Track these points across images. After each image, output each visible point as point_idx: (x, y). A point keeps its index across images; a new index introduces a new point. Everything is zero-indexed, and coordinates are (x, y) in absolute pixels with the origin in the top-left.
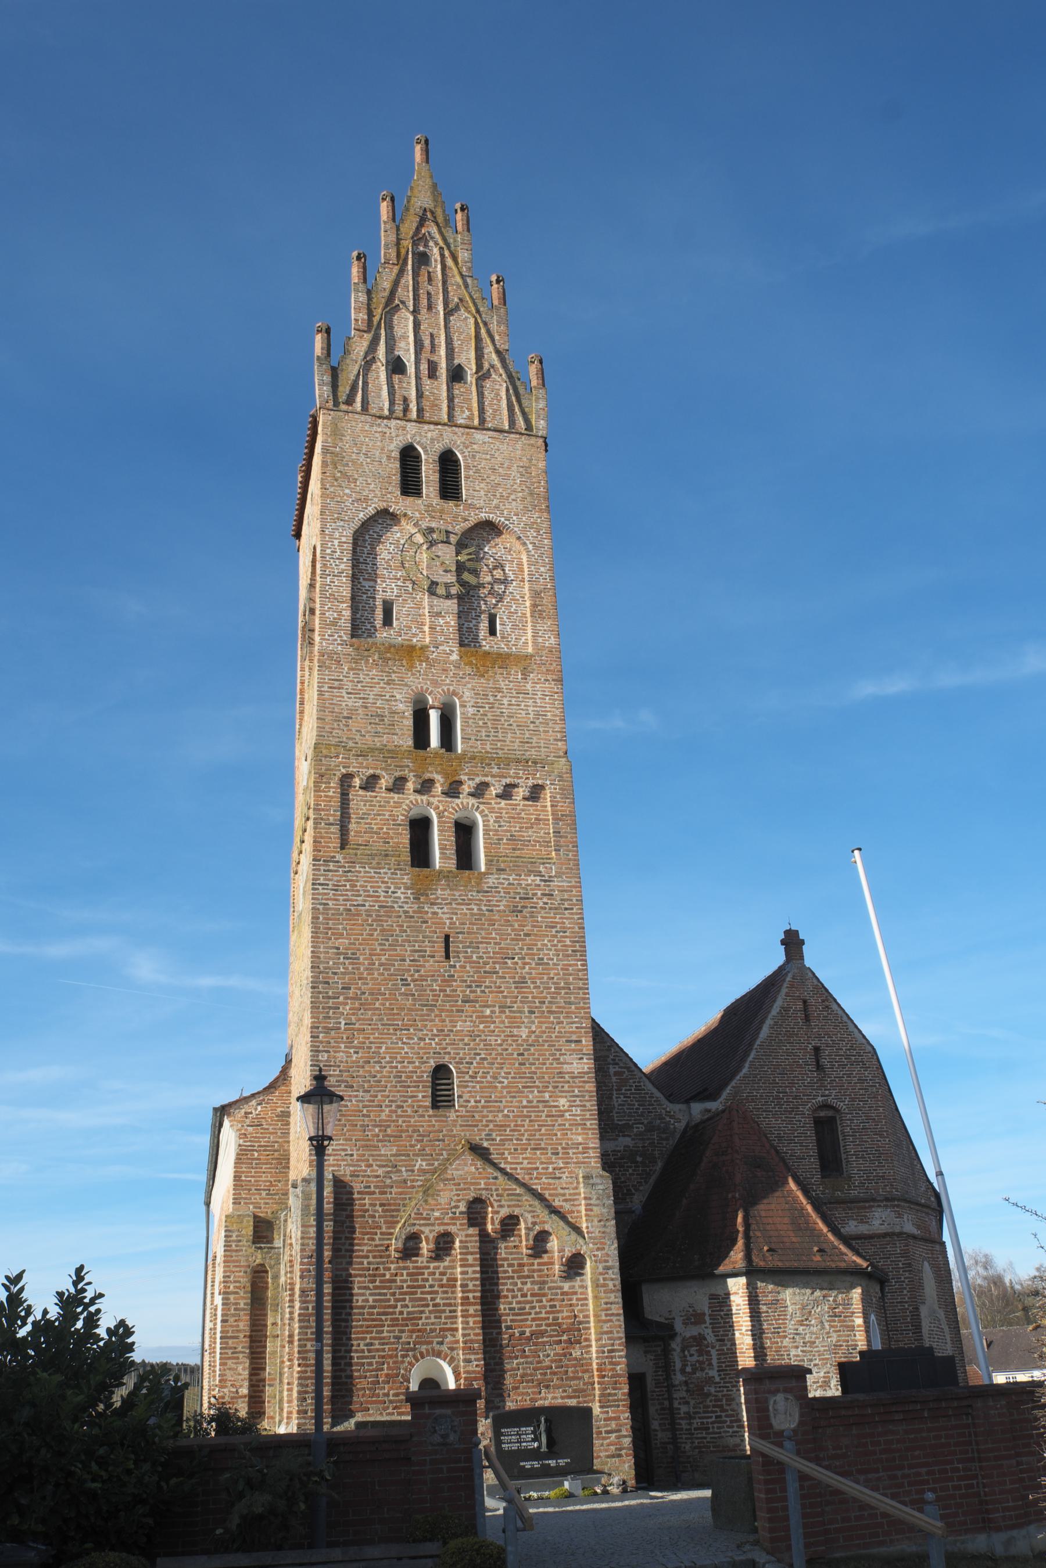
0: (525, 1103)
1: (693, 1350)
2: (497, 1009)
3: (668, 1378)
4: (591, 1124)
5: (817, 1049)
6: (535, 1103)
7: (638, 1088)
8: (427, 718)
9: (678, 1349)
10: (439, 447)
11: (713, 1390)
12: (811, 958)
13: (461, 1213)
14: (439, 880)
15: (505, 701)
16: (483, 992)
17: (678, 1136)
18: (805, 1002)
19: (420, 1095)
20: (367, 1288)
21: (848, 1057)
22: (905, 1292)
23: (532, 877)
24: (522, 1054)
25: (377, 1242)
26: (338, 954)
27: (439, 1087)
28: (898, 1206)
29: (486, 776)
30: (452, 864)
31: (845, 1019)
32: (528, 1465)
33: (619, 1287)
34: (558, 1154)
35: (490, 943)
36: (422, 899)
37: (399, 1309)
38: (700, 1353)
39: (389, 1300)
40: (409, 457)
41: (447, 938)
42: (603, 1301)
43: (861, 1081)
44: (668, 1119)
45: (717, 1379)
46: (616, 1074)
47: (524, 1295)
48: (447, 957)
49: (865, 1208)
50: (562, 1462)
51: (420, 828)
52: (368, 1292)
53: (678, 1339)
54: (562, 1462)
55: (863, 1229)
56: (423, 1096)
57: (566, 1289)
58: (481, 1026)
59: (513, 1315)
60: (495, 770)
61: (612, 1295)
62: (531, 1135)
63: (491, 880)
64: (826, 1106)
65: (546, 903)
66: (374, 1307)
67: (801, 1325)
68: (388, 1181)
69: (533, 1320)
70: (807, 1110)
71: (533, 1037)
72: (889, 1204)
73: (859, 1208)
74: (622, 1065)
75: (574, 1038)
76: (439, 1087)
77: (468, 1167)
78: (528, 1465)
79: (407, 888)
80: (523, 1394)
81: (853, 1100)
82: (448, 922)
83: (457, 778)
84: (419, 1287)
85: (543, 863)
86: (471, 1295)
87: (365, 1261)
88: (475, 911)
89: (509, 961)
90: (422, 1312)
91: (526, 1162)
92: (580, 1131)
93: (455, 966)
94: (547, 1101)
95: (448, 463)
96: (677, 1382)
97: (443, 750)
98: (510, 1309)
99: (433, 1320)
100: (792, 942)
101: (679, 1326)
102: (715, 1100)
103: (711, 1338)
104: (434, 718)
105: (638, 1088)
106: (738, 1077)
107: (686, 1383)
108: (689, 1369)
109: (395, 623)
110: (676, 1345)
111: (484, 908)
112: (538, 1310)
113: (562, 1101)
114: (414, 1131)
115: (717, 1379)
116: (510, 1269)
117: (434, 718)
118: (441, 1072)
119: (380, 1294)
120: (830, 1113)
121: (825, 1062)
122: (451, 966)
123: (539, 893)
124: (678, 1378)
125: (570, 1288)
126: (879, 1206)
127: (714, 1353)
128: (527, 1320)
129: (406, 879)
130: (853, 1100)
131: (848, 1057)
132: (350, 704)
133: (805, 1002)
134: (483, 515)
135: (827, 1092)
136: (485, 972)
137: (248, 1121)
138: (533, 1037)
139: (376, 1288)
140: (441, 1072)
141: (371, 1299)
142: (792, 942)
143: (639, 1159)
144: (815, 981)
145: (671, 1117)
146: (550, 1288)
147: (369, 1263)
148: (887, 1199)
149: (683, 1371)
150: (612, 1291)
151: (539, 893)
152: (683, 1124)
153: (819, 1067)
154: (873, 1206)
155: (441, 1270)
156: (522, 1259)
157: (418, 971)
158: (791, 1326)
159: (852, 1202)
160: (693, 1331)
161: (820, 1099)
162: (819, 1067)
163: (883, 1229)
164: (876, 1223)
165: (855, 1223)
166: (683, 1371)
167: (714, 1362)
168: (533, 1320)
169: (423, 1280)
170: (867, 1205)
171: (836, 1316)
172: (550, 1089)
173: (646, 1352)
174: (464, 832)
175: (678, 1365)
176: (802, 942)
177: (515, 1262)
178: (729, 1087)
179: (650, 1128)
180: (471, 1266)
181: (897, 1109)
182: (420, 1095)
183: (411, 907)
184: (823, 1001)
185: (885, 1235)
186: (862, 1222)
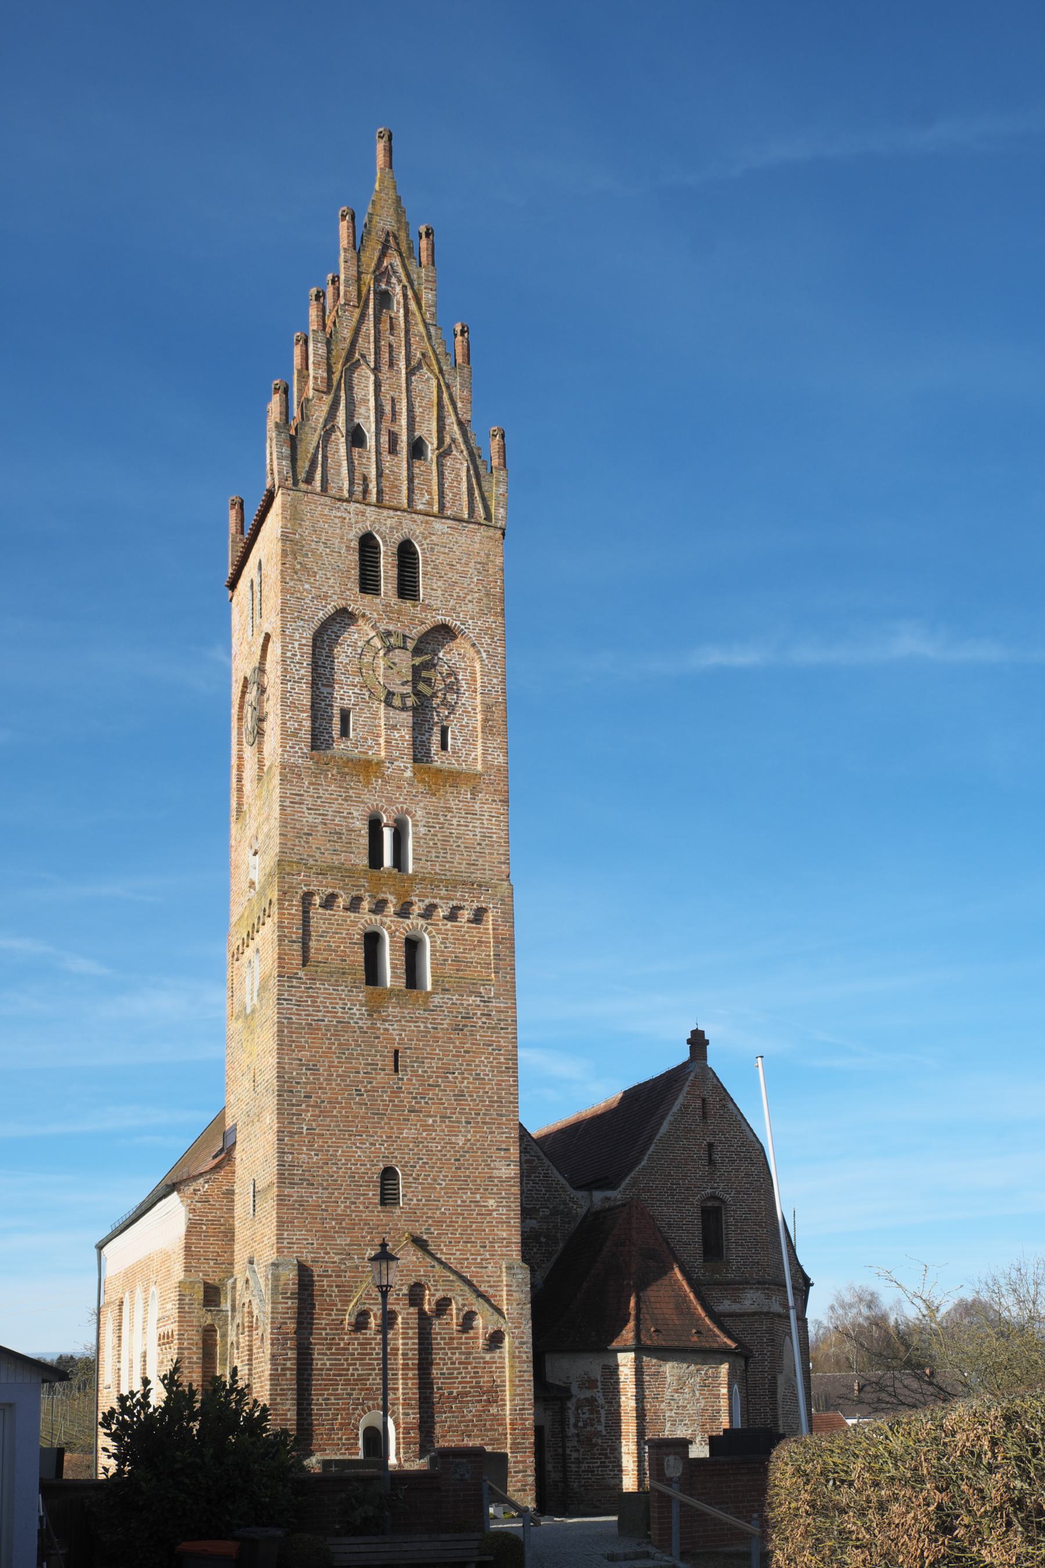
0: (459, 1203)
1: (585, 1409)
2: (438, 1119)
5: (710, 1146)
6: (468, 1203)
9: (573, 1408)
10: (398, 537)
11: (599, 1441)
13: (404, 1295)
14: (391, 998)
17: (579, 1220)
18: (704, 1100)
19: (371, 1193)
22: (766, 1363)
23: (473, 998)
24: (458, 1160)
25: (334, 1317)
28: (768, 1289)
29: (435, 898)
30: (402, 983)
33: (531, 1359)
34: (485, 1247)
35: (434, 1059)
38: (591, 1412)
39: (343, 1364)
40: (367, 545)
41: (396, 1052)
42: (517, 1369)
43: (747, 1175)
44: (571, 1205)
45: (604, 1433)
47: (453, 1363)
48: (396, 1070)
49: (739, 1289)
51: (372, 941)
52: (326, 1357)
53: (574, 1400)
55: (736, 1308)
56: (373, 1194)
57: (487, 1359)
58: (424, 1134)
60: (443, 892)
61: (525, 1365)
62: (463, 1230)
63: (437, 1000)
64: (713, 1197)
65: (485, 1023)
67: (677, 1393)
69: (460, 1383)
70: (696, 1200)
71: (468, 1145)
72: (760, 1286)
73: (733, 1289)
74: (532, 1153)
81: (738, 1192)
82: (397, 1038)
83: (408, 899)
84: (368, 1354)
85: (484, 985)
86: (410, 1362)
87: (324, 1333)
88: (422, 1028)
89: (450, 1076)
90: (370, 1374)
92: (505, 1228)
93: (402, 1079)
94: (478, 1202)
95: (406, 553)
98: (441, 1374)
101: (574, 1390)
102: (614, 1188)
103: (601, 1400)
104: (387, 834)
106: (637, 1169)
107: (578, 1435)
108: (581, 1424)
110: (571, 1405)
112: (463, 1375)
113: (491, 1202)
114: (365, 1224)
115: (604, 1433)
116: (442, 1342)
117: (387, 834)
118: (389, 1174)
119: (335, 1359)
120: (717, 1204)
121: (717, 1157)
122: (399, 1079)
124: (572, 1431)
126: (752, 1288)
127: (603, 1412)
128: (455, 1383)
129: (361, 997)
130: (738, 1192)
133: (704, 1100)
134: (439, 617)
135: (716, 1185)
137: (197, 1198)
138: (468, 1145)
139: (332, 1354)
140: (389, 1174)
141: (328, 1363)
143: (543, 1240)
144: (715, 1080)
146: (474, 1358)
148: (759, 1283)
149: (576, 1426)
150: (525, 1362)
151: (479, 1013)
152: (585, 1210)
153: (711, 1162)
154: (746, 1288)
156: (453, 1334)
157: (371, 1083)
158: (668, 1393)
159: (728, 1284)
160: (588, 1394)
161: (709, 1191)
162: (711, 1162)
163: (754, 1308)
164: (748, 1303)
165: (729, 1302)
166: (576, 1426)
167: (603, 1419)
168: (460, 1383)
169: (371, 1349)
170: (741, 1287)
171: (705, 1386)
172: (481, 1191)
174: (412, 947)
175: (572, 1421)
177: (447, 1336)
178: (628, 1178)
180: (411, 1338)
182: (371, 1193)
184: (721, 1100)
185: (754, 1314)
186: (735, 1301)
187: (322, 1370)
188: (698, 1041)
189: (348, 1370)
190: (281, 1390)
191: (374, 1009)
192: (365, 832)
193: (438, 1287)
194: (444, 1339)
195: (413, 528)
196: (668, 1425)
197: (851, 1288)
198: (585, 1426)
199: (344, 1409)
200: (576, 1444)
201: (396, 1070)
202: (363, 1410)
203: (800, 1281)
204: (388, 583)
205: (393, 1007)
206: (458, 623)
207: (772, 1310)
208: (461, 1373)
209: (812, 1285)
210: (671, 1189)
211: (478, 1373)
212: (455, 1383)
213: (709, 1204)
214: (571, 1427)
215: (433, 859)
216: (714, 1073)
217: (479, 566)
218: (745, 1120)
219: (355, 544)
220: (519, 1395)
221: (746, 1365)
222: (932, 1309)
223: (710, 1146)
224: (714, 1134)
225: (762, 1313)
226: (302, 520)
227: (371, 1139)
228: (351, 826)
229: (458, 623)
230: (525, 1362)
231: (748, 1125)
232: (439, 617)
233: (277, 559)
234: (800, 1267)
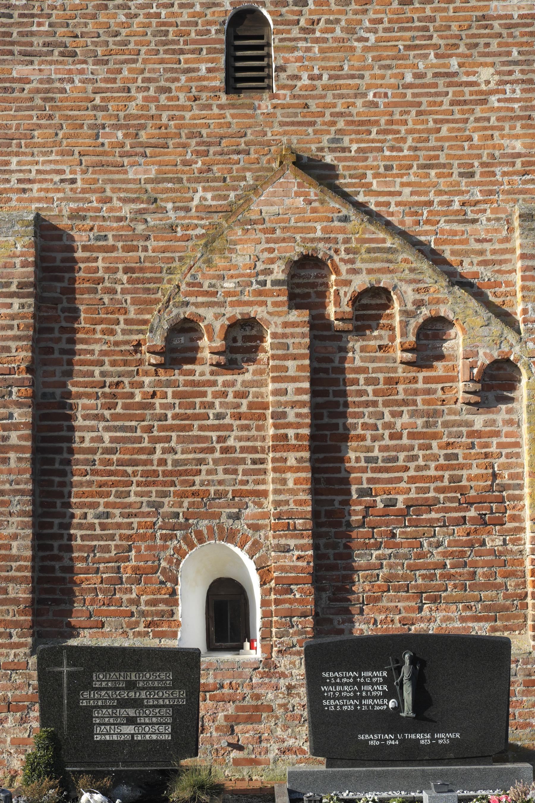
0: (409, 78)
6: (429, 79)
37: (158, 455)
39: (140, 440)
50: (443, 738)
54: (443, 738)
59: (374, 470)
66: (113, 451)
69: (412, 480)
84: (197, 417)
87: (97, 371)
91: (407, 191)
114: (191, 135)
119: (123, 429)
128: (400, 480)
168: (412, 480)
182: (203, 67)
189: (153, 451)
194: (374, 381)
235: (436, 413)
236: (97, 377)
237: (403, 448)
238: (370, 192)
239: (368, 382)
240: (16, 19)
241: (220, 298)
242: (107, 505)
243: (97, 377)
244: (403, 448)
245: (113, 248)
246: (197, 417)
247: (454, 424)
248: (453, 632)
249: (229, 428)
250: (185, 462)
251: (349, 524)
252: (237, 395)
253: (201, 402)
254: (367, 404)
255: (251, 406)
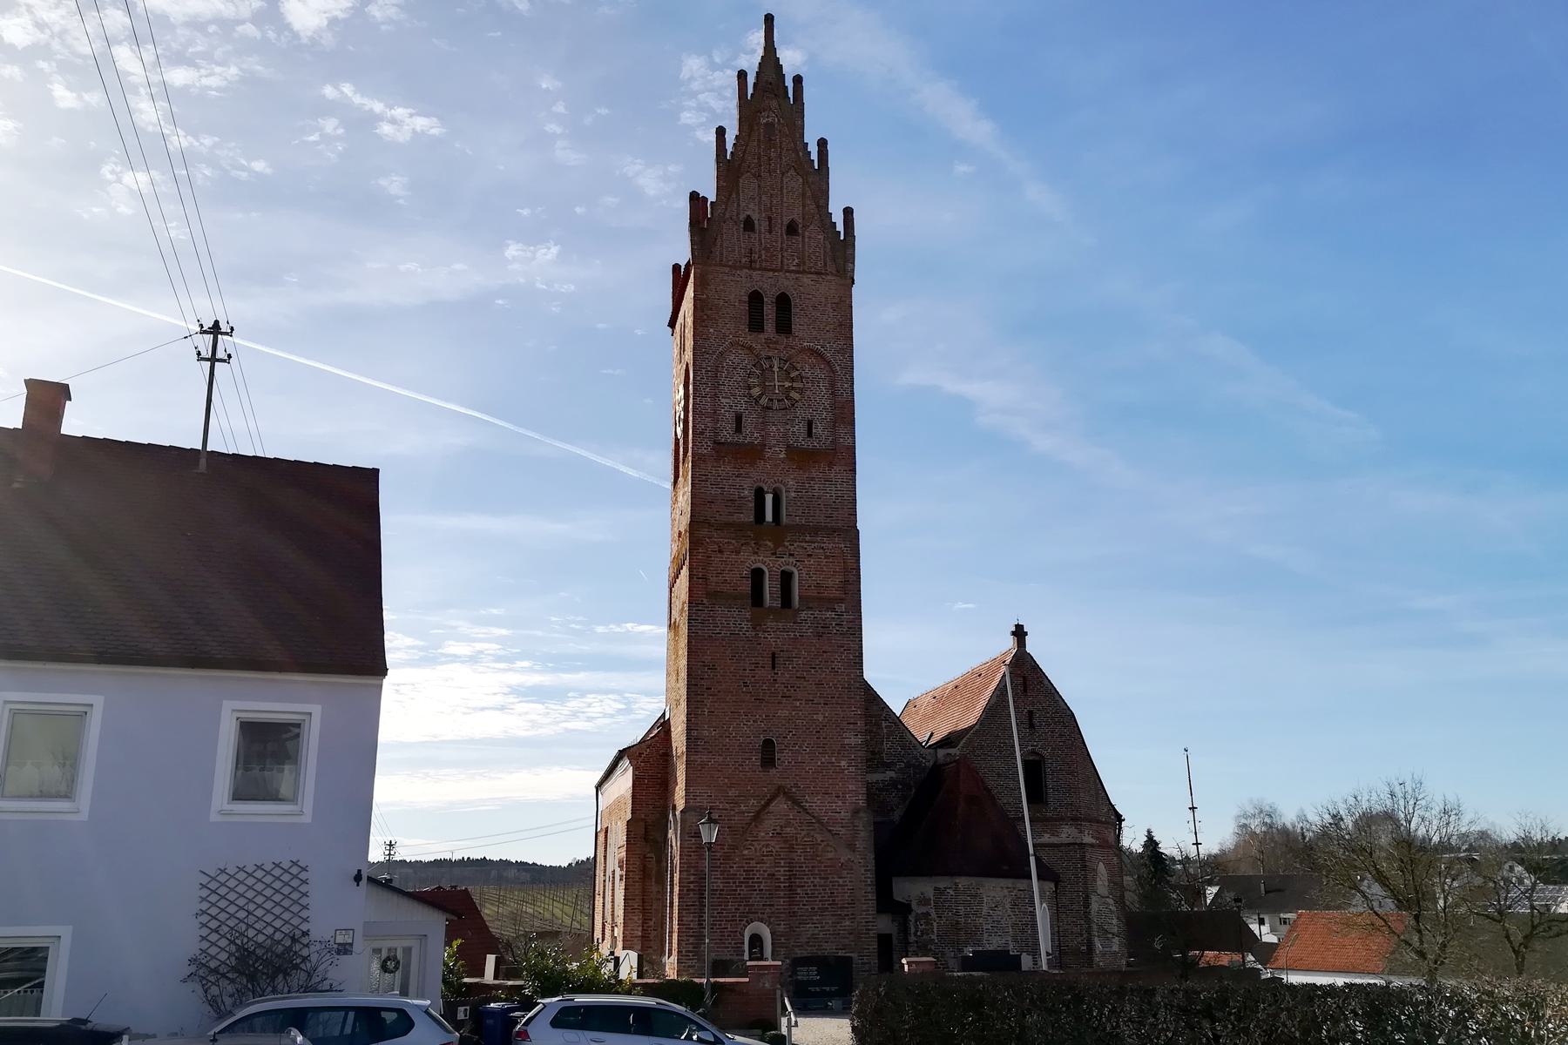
0: (819, 764)
1: (922, 922)
2: (803, 702)
3: (906, 938)
4: (784, 902)
5: (1031, 713)
6: (826, 764)
7: (901, 737)
8: (764, 500)
9: (913, 920)
10: (775, 292)
11: (933, 947)
12: (1030, 648)
15: (816, 487)
16: (795, 690)
17: (927, 771)
19: (754, 758)
20: (719, 878)
21: (1052, 718)
25: (726, 850)
26: (704, 666)
27: (769, 517)
29: (802, 542)
30: (778, 604)
31: (1053, 691)
32: (812, 989)
33: (874, 883)
36: (758, 628)
37: (738, 892)
38: (927, 923)
39: (732, 886)
40: (755, 298)
41: (774, 654)
44: (921, 759)
45: (936, 941)
46: (886, 727)
47: (815, 886)
48: (774, 668)
50: (833, 989)
51: (757, 575)
53: (913, 914)
54: (833, 989)
55: (1055, 840)
56: (756, 759)
57: (841, 883)
58: (794, 713)
59: (808, 897)
60: (808, 538)
61: (870, 888)
63: (803, 615)
66: (723, 890)
68: (732, 813)
69: (820, 901)
74: (890, 721)
75: (852, 726)
76: (769, 517)
77: (780, 805)
78: (812, 989)
79: (747, 621)
80: (811, 946)
84: (751, 879)
87: (719, 862)
89: (813, 670)
90: (753, 894)
91: (819, 801)
93: (777, 674)
95: (783, 302)
96: (911, 941)
97: (774, 524)
99: (758, 899)
100: (1019, 633)
101: (914, 906)
102: (955, 747)
103: (934, 915)
104: (769, 498)
105: (901, 737)
107: (917, 942)
108: (919, 933)
109: (743, 430)
110: (911, 918)
111: (798, 635)
112: (823, 895)
113: (843, 763)
114: (749, 781)
115: (936, 941)
116: (807, 869)
117: (769, 498)
118: (768, 744)
119: (726, 883)
120: (1037, 758)
121: (1035, 721)
122: (775, 674)
123: (834, 623)
124: (912, 938)
125: (844, 882)
127: (935, 924)
128: (816, 901)
129: (748, 615)
130: (1053, 749)
131: (1052, 718)
132: (713, 493)
133: (1024, 678)
136: (797, 677)
137: (640, 759)
139: (724, 878)
140: (768, 744)
142: (1019, 633)
143: (900, 787)
145: (923, 758)
146: (831, 882)
147: (721, 863)
149: (915, 934)
151: (834, 623)
152: (931, 763)
155: (765, 869)
158: (985, 910)
160: (922, 909)
163: (1070, 840)
164: (1063, 835)
165: (1048, 835)
166: (915, 934)
167: (935, 930)
168: (820, 901)
169: (753, 874)
173: (893, 921)
174: (786, 577)
175: (913, 930)
176: (1026, 634)
179: (908, 765)
181: (1089, 754)
182: (754, 758)
183: (751, 634)
185: (1069, 844)
186: (1053, 835)
187: (717, 890)
188: (358, 885)
189: (736, 890)
190: (687, 906)
191: (756, 624)
192: (752, 497)
193: (804, 828)
194: (808, 867)
195: (786, 283)
196: (986, 935)
197: (1251, 801)
198: (922, 934)
199: (733, 921)
200: (915, 949)
201: (774, 668)
202: (747, 921)
203: (1113, 817)
204: (770, 326)
205: (771, 622)
206: (819, 347)
207: (1084, 842)
208: (820, 894)
209: (1124, 820)
210: (999, 746)
211: (833, 893)
212: (816, 901)
213: (1031, 758)
214: (912, 935)
215: (800, 514)
216: (1032, 657)
217: (834, 305)
218: (1058, 693)
219: (746, 299)
220: (864, 911)
221: (1056, 888)
222: (1337, 818)
223: (1031, 713)
224: (1033, 704)
225: (1076, 844)
226: (708, 285)
227: (754, 718)
228: (742, 495)
229: (819, 347)
230: (869, 885)
231: (1061, 697)
232: (805, 344)
233: (691, 312)
234: (1113, 806)
235: (828, 878)
236: (718, 865)
237: (817, 890)
238: (807, 802)
239: (806, 867)
240: (693, 740)
241: (759, 838)
242: (722, 909)
243: (718, 865)
244: (817, 890)
245: (724, 820)
246: (751, 879)
247: (834, 882)
248: (30, 662)
249: (761, 882)
250: (747, 894)
251: (560, 973)
252: (764, 871)
253: (761, 958)
254: (805, 875)
255: (768, 875)
